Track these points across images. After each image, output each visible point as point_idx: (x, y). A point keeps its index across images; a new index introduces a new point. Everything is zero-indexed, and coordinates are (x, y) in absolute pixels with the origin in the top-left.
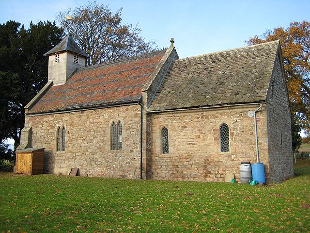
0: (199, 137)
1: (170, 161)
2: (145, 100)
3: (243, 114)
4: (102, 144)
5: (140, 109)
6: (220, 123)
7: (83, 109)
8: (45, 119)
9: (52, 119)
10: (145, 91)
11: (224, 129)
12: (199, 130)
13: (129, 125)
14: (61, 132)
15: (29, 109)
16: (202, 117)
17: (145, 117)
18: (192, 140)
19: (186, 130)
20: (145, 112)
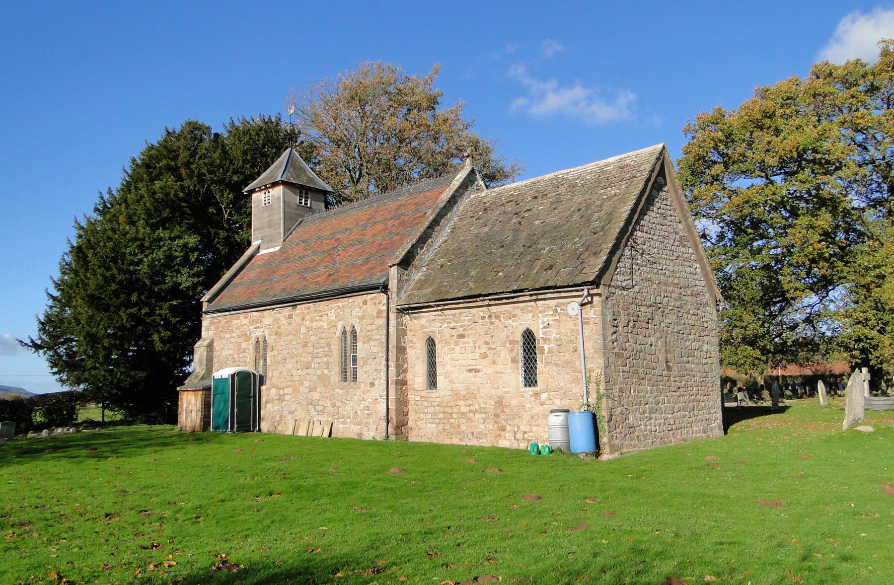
0: (484, 356)
1: (438, 405)
2: (393, 285)
3: (559, 309)
4: (326, 371)
5: (385, 301)
6: (522, 329)
7: (293, 301)
8: (235, 322)
9: (246, 321)
10: (393, 265)
11: (529, 338)
12: (486, 343)
13: (368, 334)
14: (262, 346)
15: (210, 301)
16: (490, 317)
17: (392, 316)
18: (474, 362)
19: (464, 343)
20: (393, 307)
